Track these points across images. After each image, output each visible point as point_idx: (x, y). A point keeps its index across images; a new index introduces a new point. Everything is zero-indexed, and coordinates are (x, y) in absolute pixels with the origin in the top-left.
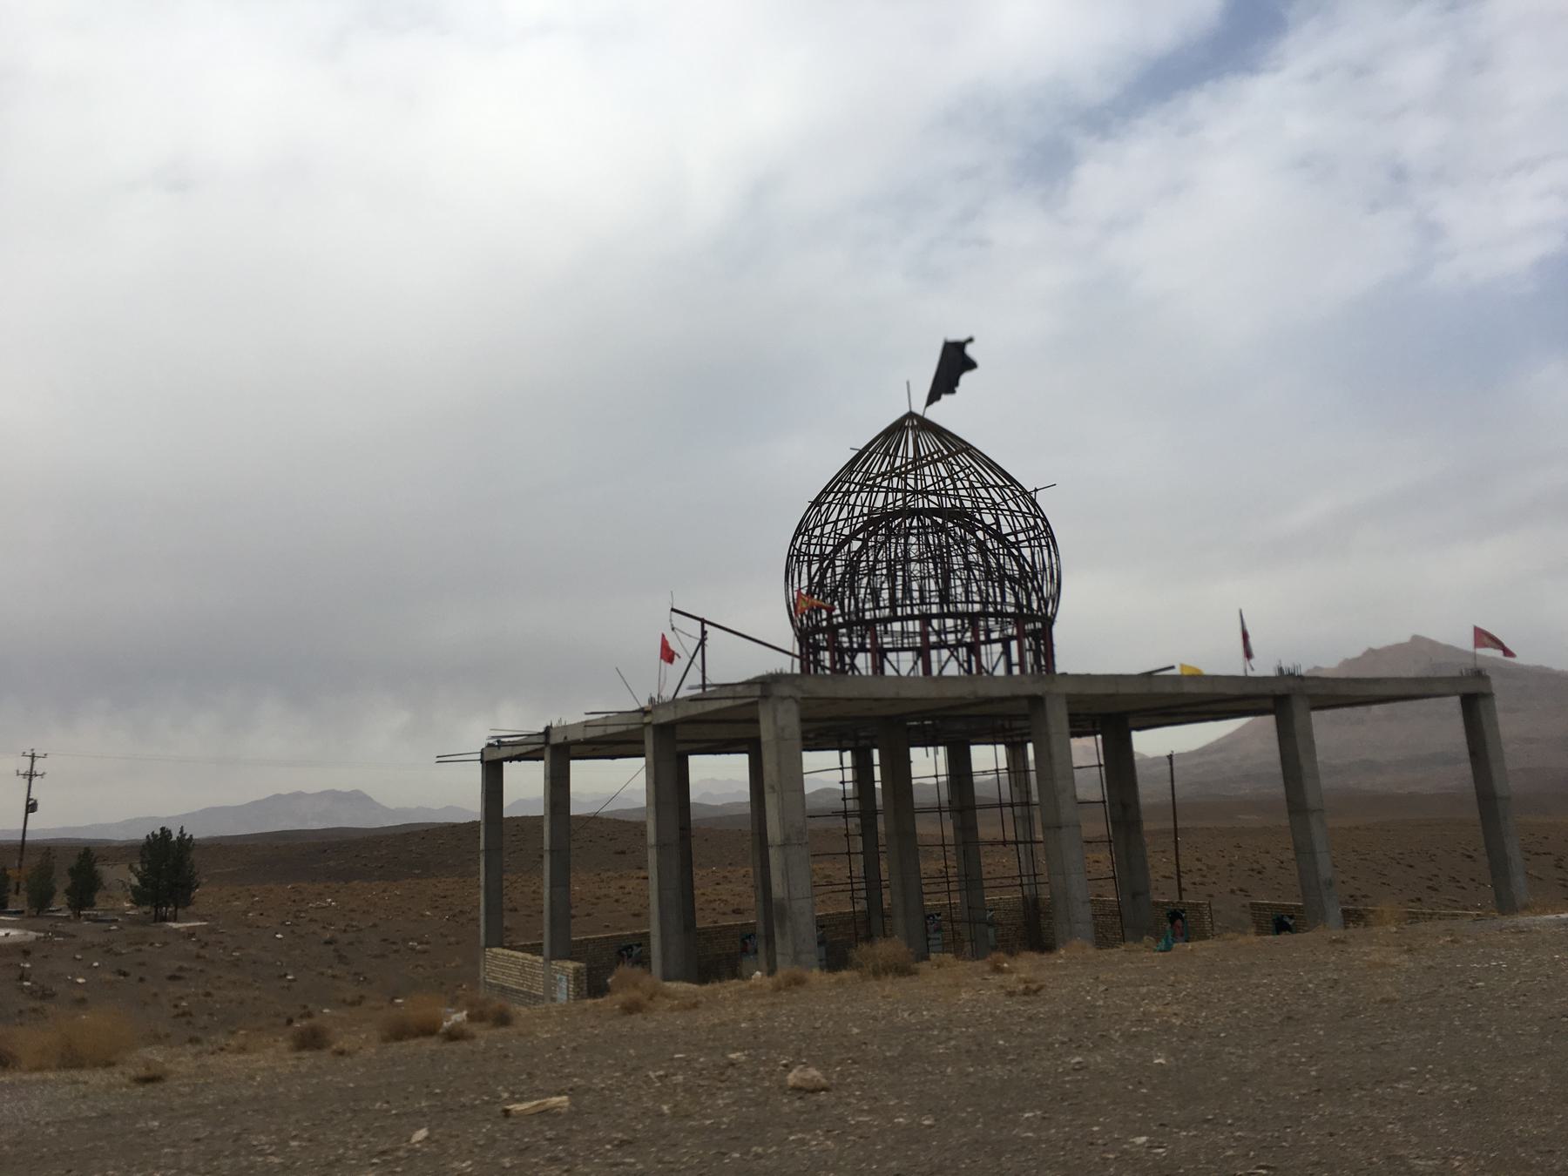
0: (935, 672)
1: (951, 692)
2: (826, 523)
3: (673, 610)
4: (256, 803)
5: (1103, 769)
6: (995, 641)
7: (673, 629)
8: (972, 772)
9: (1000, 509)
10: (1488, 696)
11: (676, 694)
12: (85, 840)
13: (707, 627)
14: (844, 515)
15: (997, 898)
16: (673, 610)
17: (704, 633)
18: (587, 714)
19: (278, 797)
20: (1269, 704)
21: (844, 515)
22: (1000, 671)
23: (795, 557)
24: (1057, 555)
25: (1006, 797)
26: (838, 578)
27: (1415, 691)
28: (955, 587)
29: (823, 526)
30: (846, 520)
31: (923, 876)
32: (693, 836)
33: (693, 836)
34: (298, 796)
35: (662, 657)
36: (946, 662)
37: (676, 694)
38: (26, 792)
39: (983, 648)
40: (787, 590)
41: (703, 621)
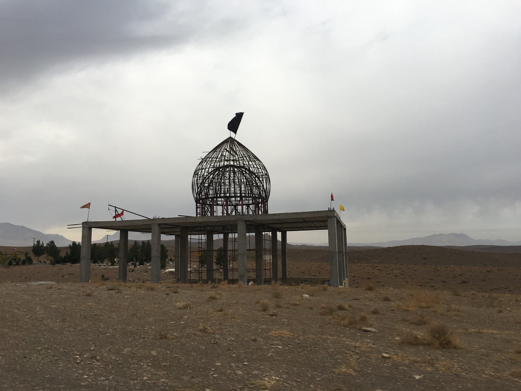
3: (109, 205)
4: (397, 247)
7: (109, 209)
8: (213, 241)
9: (245, 161)
13: (116, 208)
14: (210, 160)
16: (109, 205)
17: (116, 210)
18: (179, 216)
19: (435, 235)
21: (210, 160)
23: (196, 173)
25: (206, 249)
26: (207, 180)
29: (217, 158)
30: (210, 161)
31: (255, 273)
34: (441, 235)
35: (83, 223)
38: (125, 210)
39: (215, 206)
41: (116, 207)
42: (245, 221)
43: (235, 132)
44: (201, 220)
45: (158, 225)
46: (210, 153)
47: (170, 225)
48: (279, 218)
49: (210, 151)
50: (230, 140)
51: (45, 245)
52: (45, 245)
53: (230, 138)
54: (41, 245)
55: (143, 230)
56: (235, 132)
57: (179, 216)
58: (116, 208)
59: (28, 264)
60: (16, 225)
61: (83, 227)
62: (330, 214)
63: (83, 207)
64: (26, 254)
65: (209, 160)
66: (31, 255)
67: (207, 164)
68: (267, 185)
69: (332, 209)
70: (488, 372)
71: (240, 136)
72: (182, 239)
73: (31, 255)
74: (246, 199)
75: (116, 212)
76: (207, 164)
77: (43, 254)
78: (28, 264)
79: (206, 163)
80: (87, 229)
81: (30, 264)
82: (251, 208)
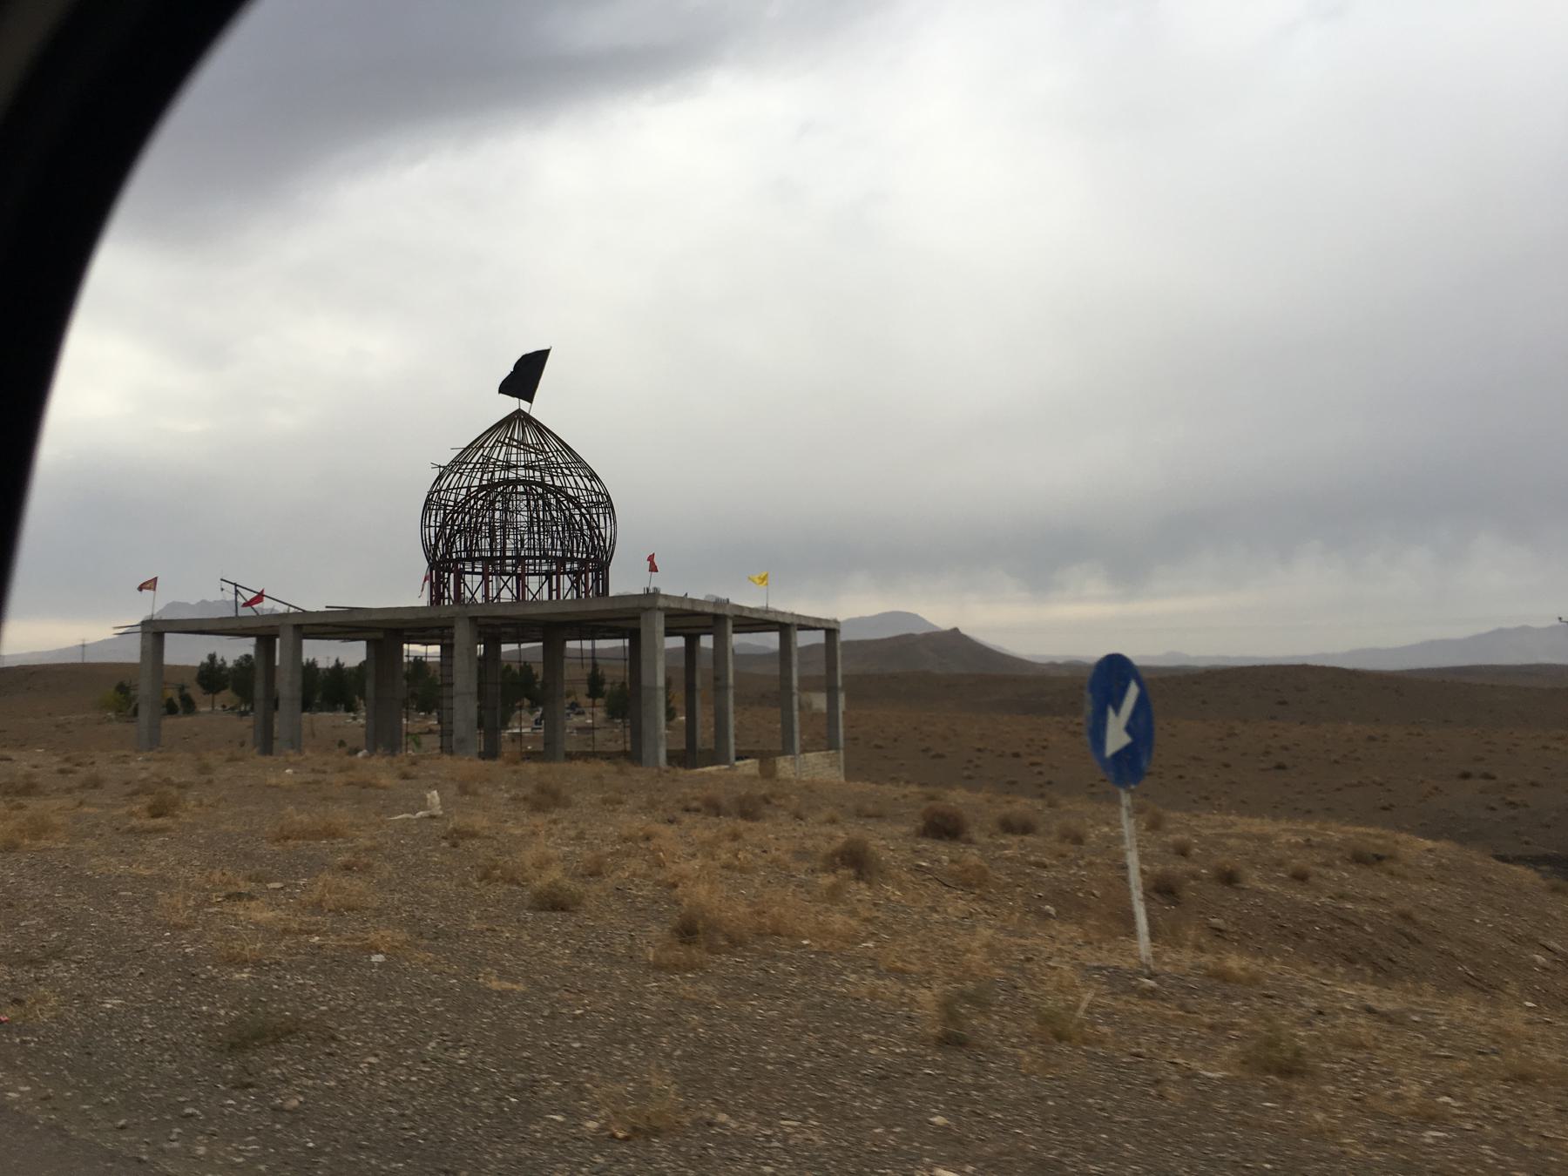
0: (562, 598)
1: (569, 609)
2: (470, 462)
3: (222, 580)
5: (627, 662)
6: (478, 573)
7: (222, 590)
10: (839, 631)
11: (242, 596)
12: (1202, 664)
15: (122, 811)
16: (222, 580)
18: (327, 607)
19: (1500, 631)
20: (777, 627)
22: (479, 597)
24: (615, 522)
27: (812, 624)
28: (436, 527)
32: (276, 739)
33: (276, 739)
34: (1525, 630)
35: (143, 623)
36: (501, 589)
37: (242, 596)
40: (615, 533)
41: (236, 585)
42: (471, 618)
43: (530, 400)
44: (434, 613)
45: (291, 628)
46: (465, 449)
47: (341, 626)
48: (398, 616)
49: (465, 447)
50: (520, 417)
51: (230, 664)
52: (230, 664)
53: (519, 412)
54: (220, 665)
55: (325, 636)
56: (530, 400)
57: (327, 607)
58: (238, 588)
59: (184, 713)
60: (315, 610)
61: (144, 632)
62: (646, 604)
63: (141, 588)
64: (182, 688)
65: (466, 468)
66: (195, 692)
67: (460, 477)
68: (427, 537)
69: (651, 591)
70: (1240, 1115)
71: (541, 408)
72: (553, 653)
73: (195, 692)
74: (572, 554)
75: (236, 595)
76: (460, 477)
77: (225, 688)
78: (184, 713)
79: (458, 475)
80: (149, 636)
81: (189, 713)
82: (469, 584)
